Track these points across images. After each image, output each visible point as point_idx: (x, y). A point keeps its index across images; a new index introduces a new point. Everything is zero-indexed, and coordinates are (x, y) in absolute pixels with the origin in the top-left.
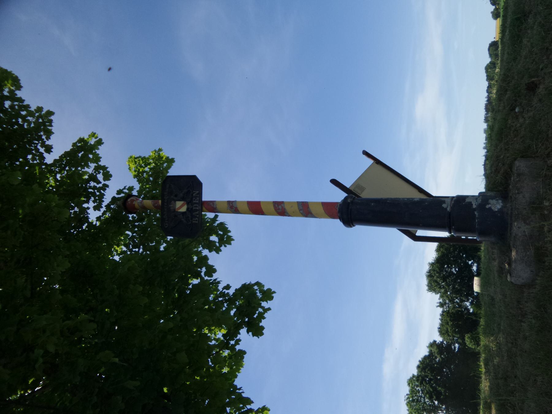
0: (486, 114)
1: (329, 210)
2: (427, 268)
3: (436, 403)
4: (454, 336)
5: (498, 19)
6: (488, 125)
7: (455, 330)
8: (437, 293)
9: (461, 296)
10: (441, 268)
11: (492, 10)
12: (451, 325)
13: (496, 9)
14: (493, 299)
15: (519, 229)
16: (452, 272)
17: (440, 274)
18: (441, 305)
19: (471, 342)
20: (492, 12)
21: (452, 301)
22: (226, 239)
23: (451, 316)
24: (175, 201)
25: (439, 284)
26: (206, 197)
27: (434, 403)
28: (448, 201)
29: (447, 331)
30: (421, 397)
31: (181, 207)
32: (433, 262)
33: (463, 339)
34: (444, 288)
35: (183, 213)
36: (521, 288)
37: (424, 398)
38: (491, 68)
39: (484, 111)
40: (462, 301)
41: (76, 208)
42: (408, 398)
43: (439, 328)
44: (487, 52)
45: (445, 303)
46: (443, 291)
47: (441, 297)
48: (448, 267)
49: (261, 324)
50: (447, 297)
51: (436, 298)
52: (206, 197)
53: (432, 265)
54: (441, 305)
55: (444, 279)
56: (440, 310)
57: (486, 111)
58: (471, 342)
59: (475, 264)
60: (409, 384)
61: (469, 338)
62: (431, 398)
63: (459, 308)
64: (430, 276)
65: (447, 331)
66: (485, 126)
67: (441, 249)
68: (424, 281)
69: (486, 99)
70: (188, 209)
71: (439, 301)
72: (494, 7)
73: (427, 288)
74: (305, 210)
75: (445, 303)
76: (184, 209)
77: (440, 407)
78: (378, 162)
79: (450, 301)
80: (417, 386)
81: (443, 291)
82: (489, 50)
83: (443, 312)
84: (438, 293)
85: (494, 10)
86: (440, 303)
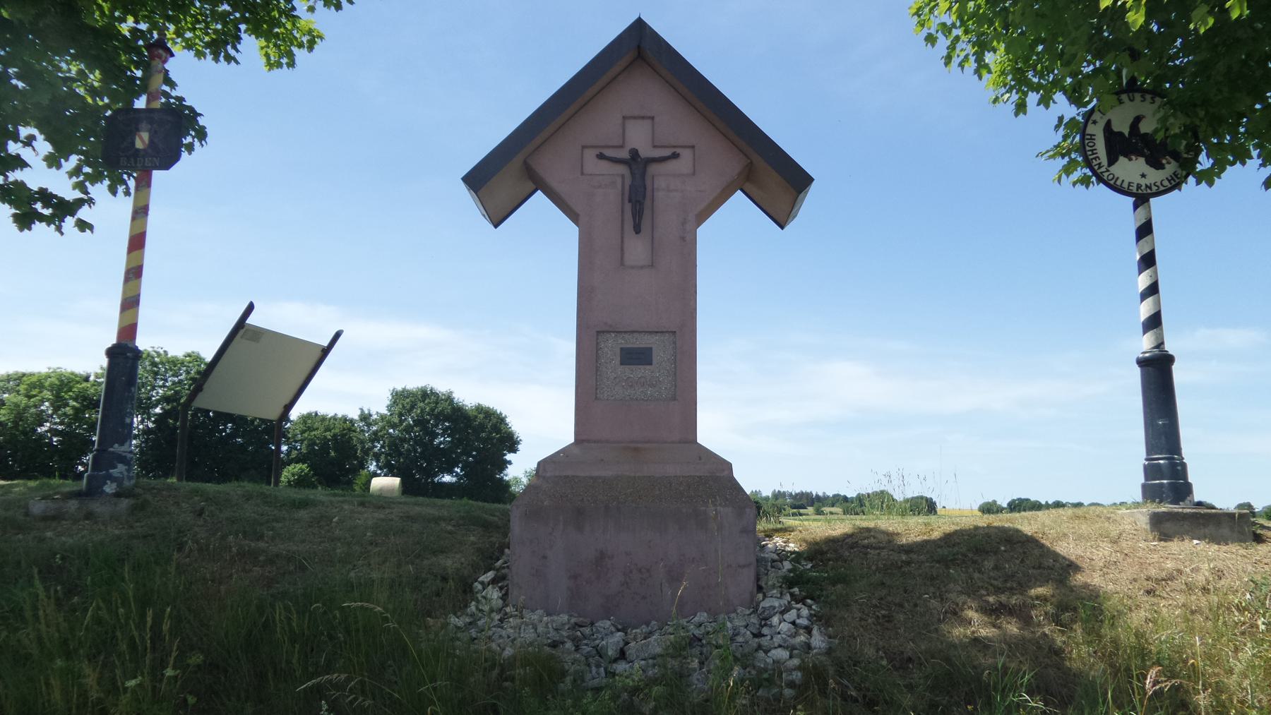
1: (128, 331)
2: (441, 387)
3: (158, 410)
4: (302, 441)
6: (767, 499)
7: (315, 444)
8: (389, 408)
9: (387, 455)
10: (440, 417)
13: (1000, 510)
18: (365, 417)
19: (293, 475)
20: (995, 502)
21: (375, 437)
23: (343, 436)
24: (150, 131)
25: (410, 411)
26: (156, 174)
27: (156, 406)
29: (310, 429)
30: (166, 380)
31: (142, 140)
33: (297, 461)
34: (401, 422)
35: (133, 143)
37: (164, 386)
39: (798, 491)
40: (377, 457)
41: (21, 128)
42: (159, 354)
45: (369, 425)
46: (396, 420)
47: (383, 417)
49: (190, 75)
50: (384, 428)
51: (379, 406)
52: (156, 174)
53: (449, 399)
54: (365, 417)
55: (420, 422)
56: (354, 415)
58: (293, 475)
60: (189, 355)
62: (166, 399)
64: (425, 394)
65: (310, 429)
67: (481, 416)
68: (413, 382)
70: (138, 150)
71: (373, 412)
73: (399, 388)
74: (130, 303)
75: (369, 425)
76: (139, 145)
77: (149, 419)
78: (326, 351)
79: (375, 433)
80: (188, 372)
81: (396, 420)
83: (352, 421)
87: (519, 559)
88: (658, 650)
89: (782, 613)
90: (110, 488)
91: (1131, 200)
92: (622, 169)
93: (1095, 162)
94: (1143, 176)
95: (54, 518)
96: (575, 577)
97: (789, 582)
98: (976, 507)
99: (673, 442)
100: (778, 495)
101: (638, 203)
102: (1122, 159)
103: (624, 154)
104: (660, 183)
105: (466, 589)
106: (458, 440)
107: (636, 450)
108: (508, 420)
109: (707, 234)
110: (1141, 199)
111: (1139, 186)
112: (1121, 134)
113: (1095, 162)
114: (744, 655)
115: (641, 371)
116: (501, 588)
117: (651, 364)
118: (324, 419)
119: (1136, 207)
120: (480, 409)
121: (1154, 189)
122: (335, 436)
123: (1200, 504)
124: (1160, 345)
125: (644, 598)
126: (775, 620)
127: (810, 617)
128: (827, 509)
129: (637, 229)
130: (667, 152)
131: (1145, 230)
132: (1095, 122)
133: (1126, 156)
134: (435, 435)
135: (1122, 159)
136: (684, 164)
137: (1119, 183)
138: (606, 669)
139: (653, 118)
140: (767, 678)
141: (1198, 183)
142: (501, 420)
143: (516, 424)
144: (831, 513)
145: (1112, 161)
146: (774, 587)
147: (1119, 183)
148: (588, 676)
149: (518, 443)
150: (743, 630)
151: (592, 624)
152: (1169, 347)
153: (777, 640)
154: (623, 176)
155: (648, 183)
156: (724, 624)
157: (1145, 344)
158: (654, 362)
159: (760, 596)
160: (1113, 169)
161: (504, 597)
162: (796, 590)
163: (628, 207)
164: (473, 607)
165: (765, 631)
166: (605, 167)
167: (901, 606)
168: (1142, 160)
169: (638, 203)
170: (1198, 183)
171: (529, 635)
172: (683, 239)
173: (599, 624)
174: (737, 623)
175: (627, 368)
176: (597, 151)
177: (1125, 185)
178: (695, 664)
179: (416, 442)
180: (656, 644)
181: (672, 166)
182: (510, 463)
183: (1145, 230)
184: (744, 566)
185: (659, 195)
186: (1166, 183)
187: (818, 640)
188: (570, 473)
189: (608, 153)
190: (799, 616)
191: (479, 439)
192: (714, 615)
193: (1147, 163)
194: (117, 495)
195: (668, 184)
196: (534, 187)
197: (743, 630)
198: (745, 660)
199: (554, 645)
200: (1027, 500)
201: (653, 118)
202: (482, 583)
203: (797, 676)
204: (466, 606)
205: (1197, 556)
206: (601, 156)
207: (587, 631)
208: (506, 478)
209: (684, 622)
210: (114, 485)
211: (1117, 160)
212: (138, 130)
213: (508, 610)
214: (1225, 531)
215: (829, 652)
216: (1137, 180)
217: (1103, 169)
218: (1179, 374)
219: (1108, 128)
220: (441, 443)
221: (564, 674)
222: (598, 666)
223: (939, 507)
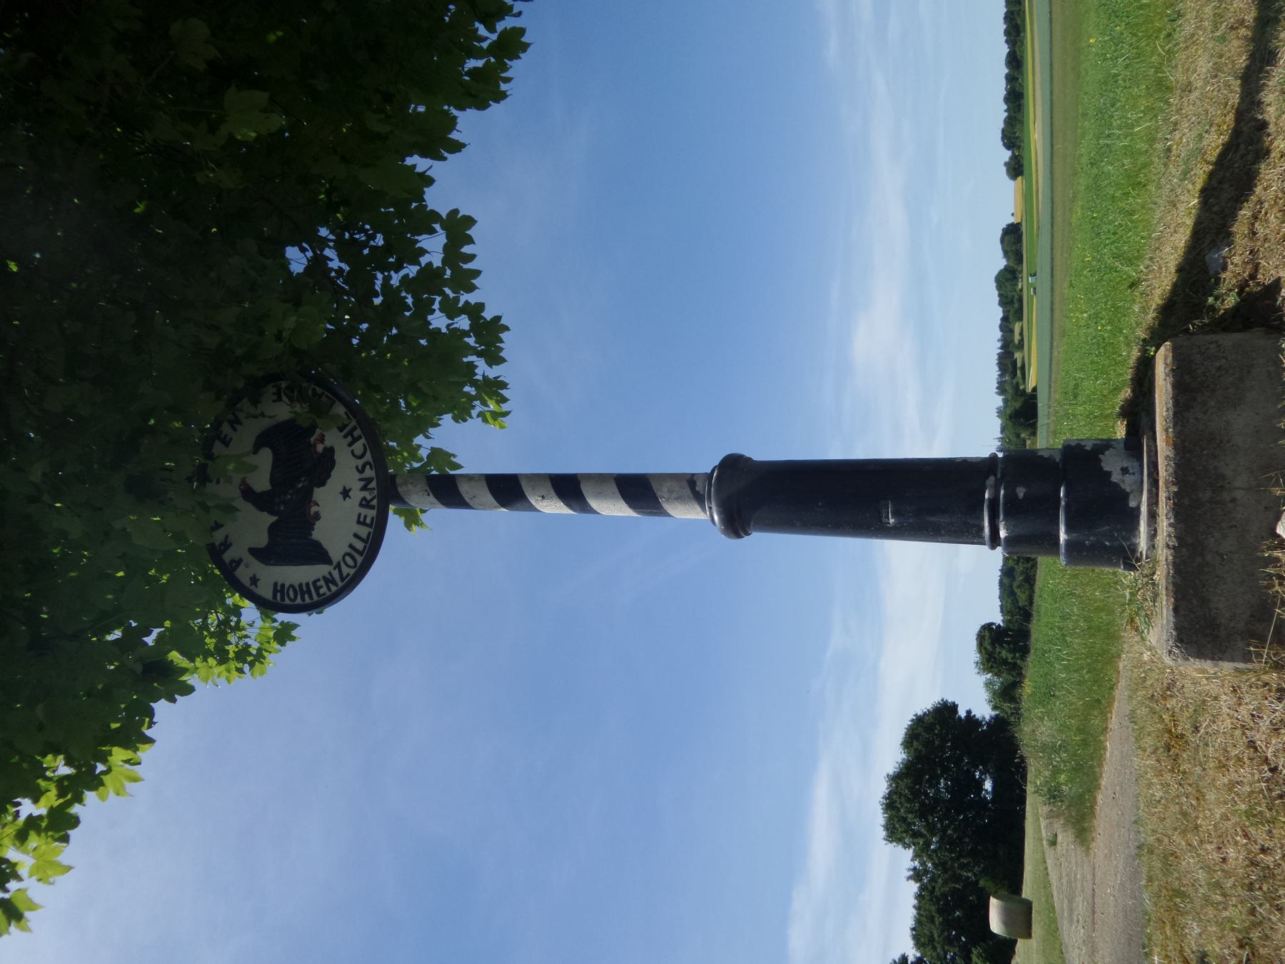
2: (882, 788)
5: (1020, 178)
6: (1005, 401)
8: (906, 846)
11: (1007, 159)
12: (941, 924)
20: (1006, 164)
22: (430, 181)
29: (931, 939)
38: (1007, 280)
43: (913, 929)
44: (999, 246)
47: (916, 856)
51: (905, 858)
53: (895, 779)
55: (923, 814)
57: (1000, 369)
61: (979, 956)
64: (891, 804)
65: (931, 939)
66: (998, 401)
67: (915, 743)
68: (877, 818)
69: (999, 344)
71: (911, 865)
72: (1009, 153)
75: (926, 871)
82: (1002, 241)
83: (922, 888)
84: (909, 847)
85: (1011, 158)
86: (915, 869)
94: (346, 493)
98: (1012, 183)
100: (1001, 389)
102: (317, 534)
108: (920, 713)
111: (365, 503)
112: (272, 529)
118: (919, 921)
121: (369, 473)
123: (1138, 412)
124: (692, 488)
128: (1017, 338)
141: (470, 240)
143: (925, 703)
144: (1021, 334)
145: (318, 554)
152: (705, 463)
157: (693, 518)
160: (336, 552)
168: (318, 493)
170: (470, 240)
177: (364, 532)
182: (969, 712)
193: (322, 483)
200: (1003, 131)
208: (987, 718)
211: (318, 545)
216: (352, 507)
217: (336, 574)
218: (772, 445)
219: (262, 555)
223: (1011, 220)
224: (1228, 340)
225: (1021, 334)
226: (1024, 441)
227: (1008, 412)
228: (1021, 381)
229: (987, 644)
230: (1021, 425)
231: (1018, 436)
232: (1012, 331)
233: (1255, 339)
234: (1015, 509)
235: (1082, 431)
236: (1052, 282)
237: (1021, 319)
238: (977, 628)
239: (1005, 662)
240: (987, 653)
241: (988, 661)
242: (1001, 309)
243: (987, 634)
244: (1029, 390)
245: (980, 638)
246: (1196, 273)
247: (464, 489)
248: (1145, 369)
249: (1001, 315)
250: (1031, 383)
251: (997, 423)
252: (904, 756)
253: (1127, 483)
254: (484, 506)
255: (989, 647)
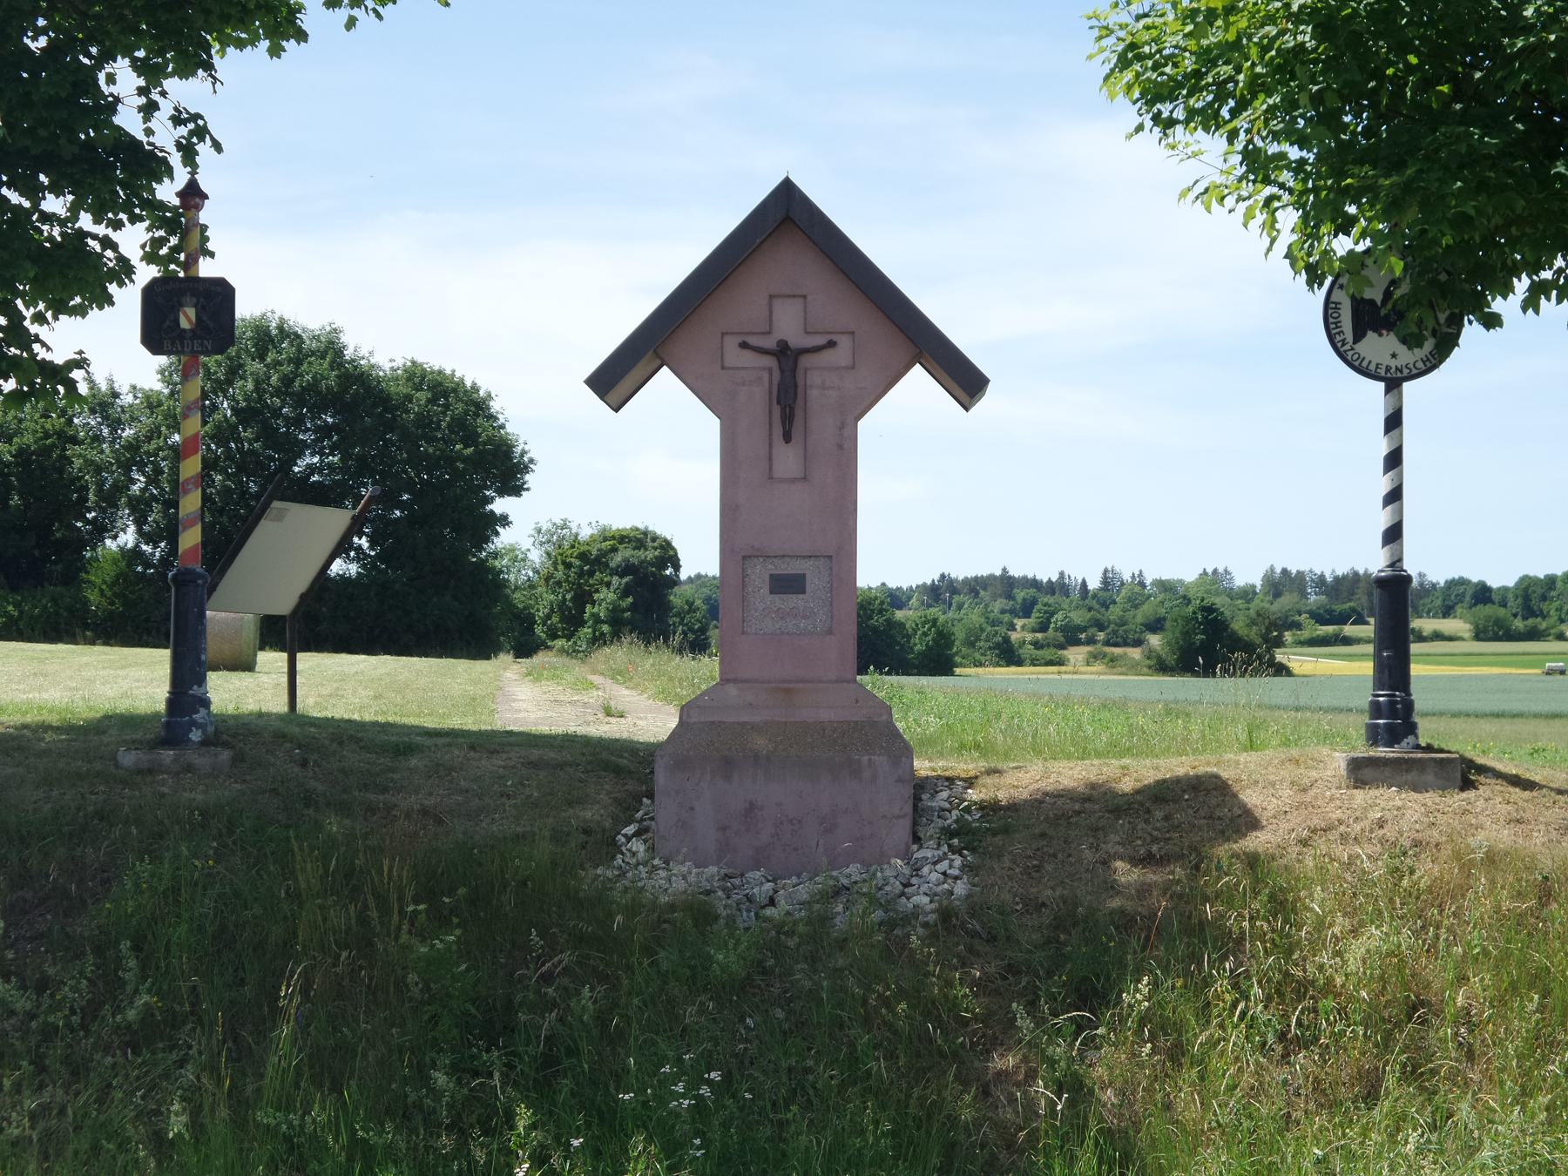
0: (1321, 579)
6: (1248, 594)
10: (313, 399)
14: (104, 733)
15: (168, 755)
16: (301, 455)
17: (277, 393)
21: (132, 456)
23: (46, 451)
24: (195, 306)
28: (201, 691)
32: (349, 354)
36: (114, 758)
47: (151, 402)
48: (325, 431)
50: (154, 433)
53: (331, 348)
59: (353, 569)
63: (100, 490)
66: (1248, 575)
67: (423, 396)
70: (184, 331)
71: (123, 386)
75: (116, 424)
76: (184, 324)
79: (133, 446)
84: (167, 381)
86: (116, 395)
87: (664, 811)
88: (805, 897)
89: (935, 863)
90: (195, 736)
91: (1382, 385)
92: (770, 362)
93: (1338, 338)
94: (1394, 356)
95: (150, 771)
96: (724, 829)
97: (949, 833)
99: (830, 682)
100: (1280, 583)
101: (788, 405)
102: (1371, 335)
103: (770, 343)
104: (815, 379)
105: (609, 847)
106: (361, 459)
107: (788, 691)
108: (495, 406)
109: (874, 429)
110: (1393, 385)
111: (1388, 369)
113: (1338, 338)
114: (888, 902)
115: (793, 601)
116: (645, 841)
117: (804, 592)
119: (1387, 391)
120: (416, 375)
121: (1406, 371)
122: (22, 453)
123: (1429, 748)
124: (1396, 563)
125: (796, 849)
126: (926, 870)
127: (963, 868)
129: (787, 438)
130: (820, 340)
131: (1394, 422)
132: (1341, 287)
133: (1375, 331)
134: (298, 450)
135: (1371, 335)
136: (840, 355)
137: (1365, 364)
138: (757, 915)
139: (805, 297)
140: (898, 922)
142: (477, 406)
144: (1438, 636)
145: (1358, 336)
146: (931, 837)
147: (1365, 364)
148: (739, 920)
149: (525, 469)
150: (892, 880)
151: (742, 875)
153: (924, 888)
154: (770, 370)
155: (800, 383)
156: (874, 874)
158: (808, 589)
159: (915, 847)
160: (1360, 347)
161: (652, 849)
162: (956, 841)
163: (777, 410)
164: (619, 860)
165: (914, 880)
166: (748, 359)
167: (1055, 856)
169: (788, 405)
171: (679, 885)
172: (840, 447)
173: (749, 875)
174: (888, 873)
175: (776, 597)
176: (740, 339)
178: (840, 908)
179: (241, 469)
180: (803, 892)
181: (827, 357)
182: (504, 520)
183: (1394, 422)
184: (899, 817)
185: (814, 394)
186: (1420, 365)
187: (960, 888)
188: (716, 718)
189: (753, 341)
190: (951, 867)
191: (416, 460)
192: (866, 865)
194: (205, 743)
195: (818, 378)
196: (658, 362)
197: (892, 880)
198: (888, 906)
199: (708, 893)
201: (805, 297)
202: (625, 836)
203: (932, 918)
204: (613, 858)
205: (1406, 809)
206: (744, 345)
207: (737, 881)
209: (835, 873)
210: (199, 733)
211: (1364, 335)
212: (182, 305)
213: (656, 862)
214: (1430, 777)
215: (968, 896)
217: (1347, 347)
220: (311, 469)
221: (717, 917)
222: (749, 911)
224: (1459, 775)
225: (1438, 636)
226: (1138, 643)
227: (1219, 601)
228: (1306, 634)
229: (623, 555)
230: (1186, 634)
231: (1155, 626)
232: (1447, 612)
233: (1459, 782)
234: (1392, 704)
235: (1420, 731)
236: (1536, 716)
237: (1480, 635)
238: (662, 529)
239: (583, 598)
240: (604, 553)
241: (583, 556)
242: (1511, 582)
243: (650, 555)
244: (1280, 656)
245: (639, 539)
246: (1483, 770)
247: (1395, 432)
248: (1441, 751)
249: (1494, 583)
250: (1300, 661)
251: (1186, 571)
252: (387, 366)
253: (1404, 744)
254: (1389, 444)
255: (617, 559)
